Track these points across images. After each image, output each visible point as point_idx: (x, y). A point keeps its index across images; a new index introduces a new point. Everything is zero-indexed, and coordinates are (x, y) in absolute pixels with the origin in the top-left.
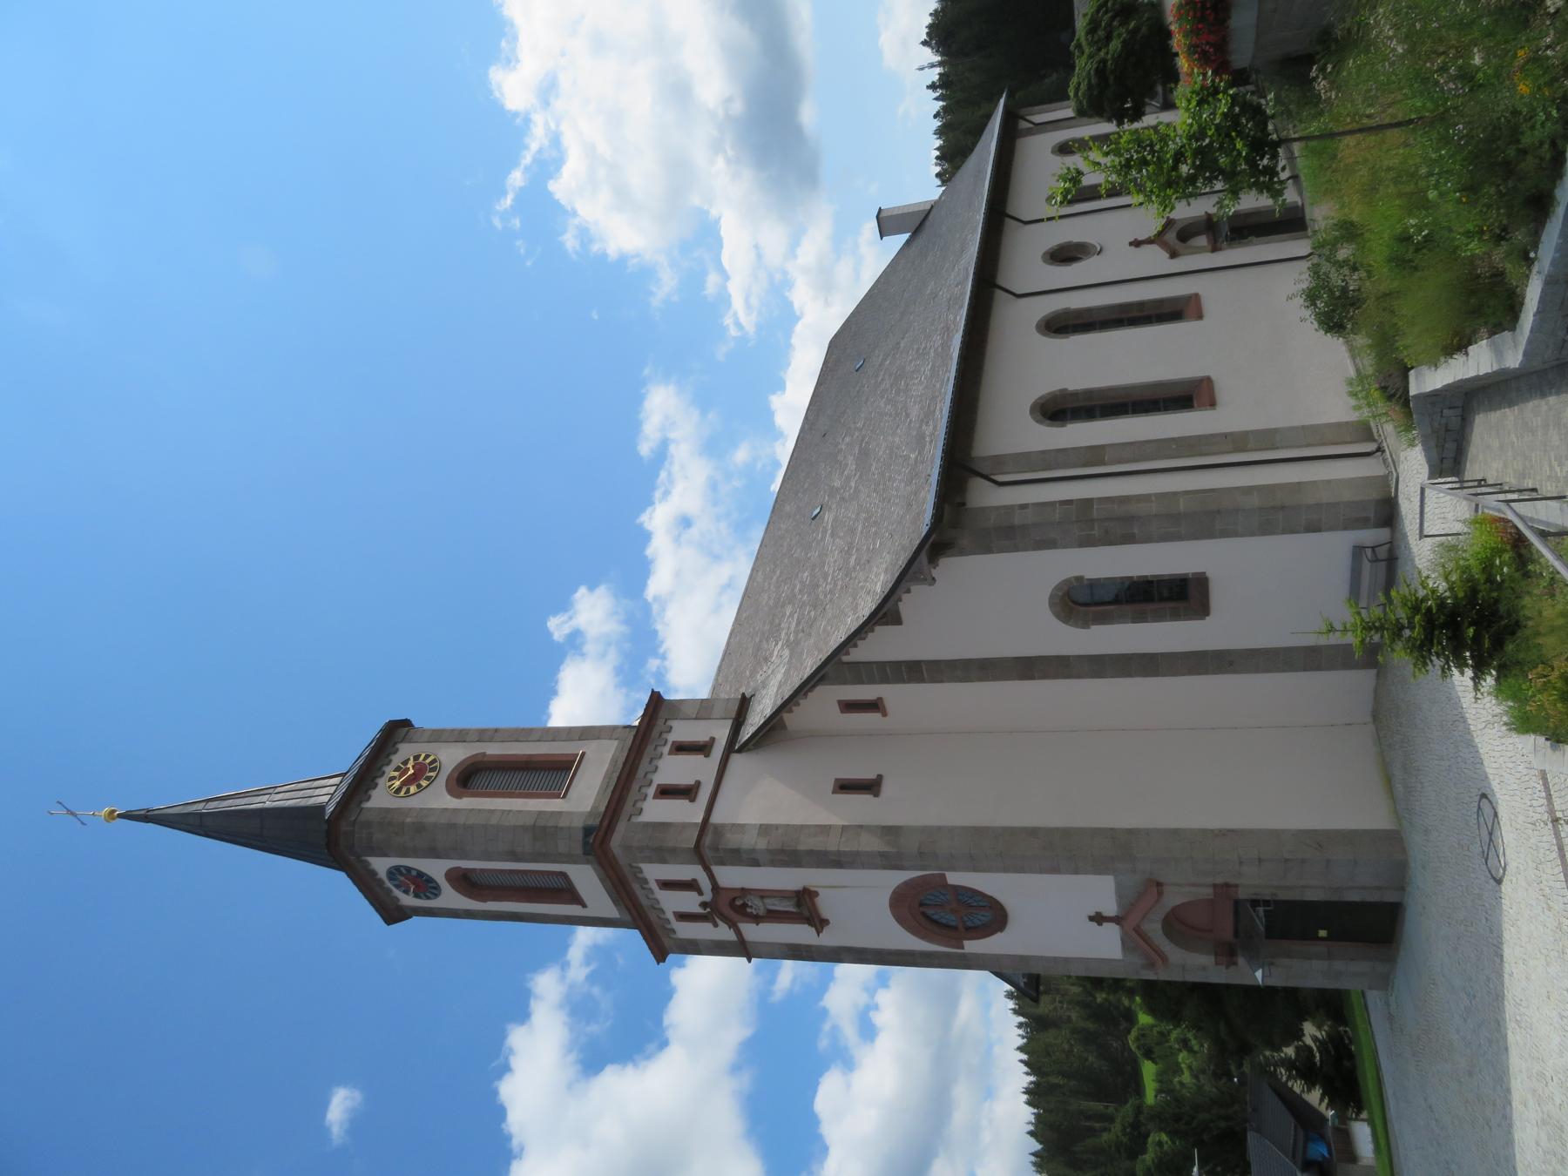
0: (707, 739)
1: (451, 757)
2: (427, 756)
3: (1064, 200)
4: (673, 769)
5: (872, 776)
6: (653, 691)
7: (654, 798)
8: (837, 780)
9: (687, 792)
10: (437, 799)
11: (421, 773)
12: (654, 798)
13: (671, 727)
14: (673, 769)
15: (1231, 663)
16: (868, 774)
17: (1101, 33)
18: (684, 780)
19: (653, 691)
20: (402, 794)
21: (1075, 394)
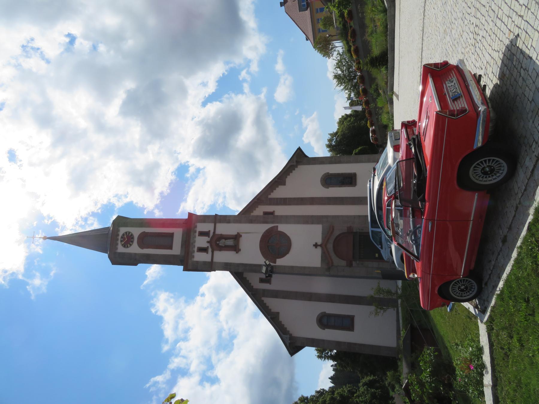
1: (136, 232)
7: (197, 252)
11: (128, 240)
20: (126, 247)
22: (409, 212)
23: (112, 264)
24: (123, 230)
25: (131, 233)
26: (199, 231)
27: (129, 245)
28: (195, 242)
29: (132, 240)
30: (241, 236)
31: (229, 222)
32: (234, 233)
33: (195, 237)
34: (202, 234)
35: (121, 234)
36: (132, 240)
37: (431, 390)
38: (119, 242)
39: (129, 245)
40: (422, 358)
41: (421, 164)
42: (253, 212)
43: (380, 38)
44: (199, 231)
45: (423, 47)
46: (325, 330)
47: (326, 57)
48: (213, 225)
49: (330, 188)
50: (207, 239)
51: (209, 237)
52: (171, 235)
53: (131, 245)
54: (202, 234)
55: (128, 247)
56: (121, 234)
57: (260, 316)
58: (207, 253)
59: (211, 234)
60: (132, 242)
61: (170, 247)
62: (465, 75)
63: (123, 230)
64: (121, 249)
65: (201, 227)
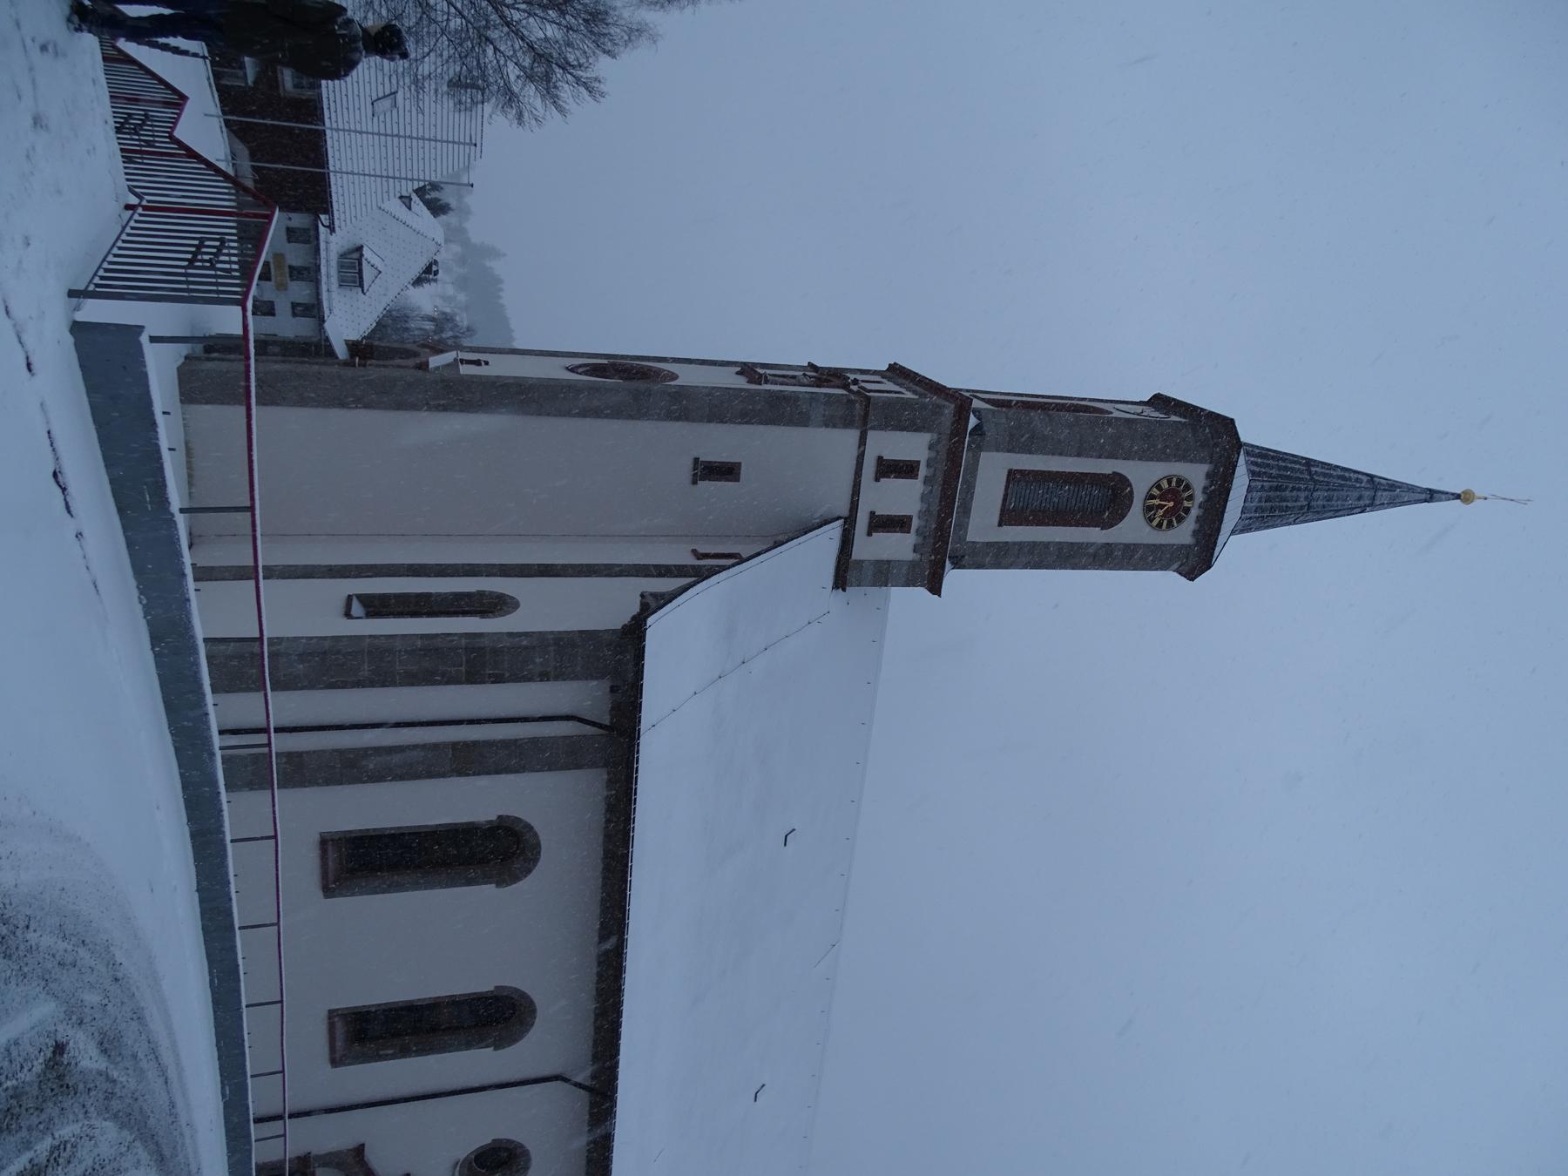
0: (883, 480)
1: (1133, 528)
2: (1160, 525)
3: (430, 22)
4: (904, 497)
5: (703, 485)
6: (940, 596)
7: (918, 462)
8: (737, 480)
9: (890, 469)
10: (1143, 475)
11: (1171, 499)
12: (918, 462)
13: (914, 551)
14: (904, 497)
15: (330, 570)
16: (708, 487)
17: (111, 963)
18: (893, 484)
19: (940, 596)
20: (1175, 479)
21: (486, 879)
22: (144, 146)
23: (1232, 420)
24: (1183, 534)
25: (1175, 476)
26: (909, 532)
27: (1165, 485)
28: (923, 498)
33: (921, 514)
38: (1199, 498)
39: (1165, 485)
44: (909, 532)
45: (19, 345)
46: (496, 987)
47: (501, 290)
49: (489, 1141)
52: (1008, 516)
58: (872, 513)
61: (1014, 477)
64: (1196, 474)
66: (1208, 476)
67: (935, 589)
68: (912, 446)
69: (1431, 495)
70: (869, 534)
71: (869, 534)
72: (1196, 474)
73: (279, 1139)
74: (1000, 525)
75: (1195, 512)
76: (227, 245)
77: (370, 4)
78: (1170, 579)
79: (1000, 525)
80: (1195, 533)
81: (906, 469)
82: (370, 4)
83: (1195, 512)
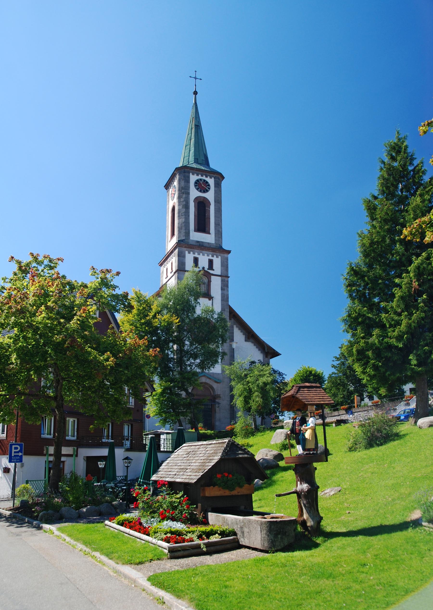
1: (210, 196)
10: (194, 193)
24: (211, 181)
29: (202, 191)
30: (210, 300)
31: (222, 289)
32: (213, 294)
34: (211, 262)
35: (208, 179)
36: (202, 191)
37: (123, 390)
38: (200, 177)
40: (250, 567)
41: (304, 508)
42: (237, 327)
43: (181, 577)
48: (220, 274)
50: (206, 267)
51: (208, 269)
53: (197, 189)
54: (211, 262)
55: (195, 186)
56: (208, 179)
57: (260, 545)
59: (211, 272)
60: (201, 191)
62: (98, 448)
63: (211, 181)
64: (193, 178)
65: (217, 262)
66: (193, 174)
67: (229, 252)
68: (189, 258)
69: (198, 127)
70: (214, 270)
71: (214, 270)
72: (193, 178)
73: (326, 429)
74: (210, 234)
75: (204, 178)
76: (12, 340)
77: (2, 326)
78: (224, 183)
79: (210, 234)
80: (211, 178)
81: (196, 261)
82: (2, 326)
83: (204, 178)
